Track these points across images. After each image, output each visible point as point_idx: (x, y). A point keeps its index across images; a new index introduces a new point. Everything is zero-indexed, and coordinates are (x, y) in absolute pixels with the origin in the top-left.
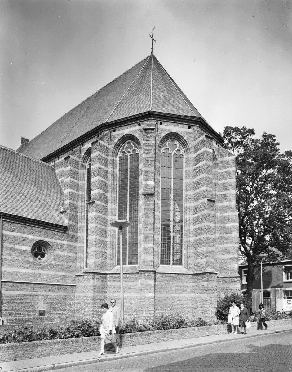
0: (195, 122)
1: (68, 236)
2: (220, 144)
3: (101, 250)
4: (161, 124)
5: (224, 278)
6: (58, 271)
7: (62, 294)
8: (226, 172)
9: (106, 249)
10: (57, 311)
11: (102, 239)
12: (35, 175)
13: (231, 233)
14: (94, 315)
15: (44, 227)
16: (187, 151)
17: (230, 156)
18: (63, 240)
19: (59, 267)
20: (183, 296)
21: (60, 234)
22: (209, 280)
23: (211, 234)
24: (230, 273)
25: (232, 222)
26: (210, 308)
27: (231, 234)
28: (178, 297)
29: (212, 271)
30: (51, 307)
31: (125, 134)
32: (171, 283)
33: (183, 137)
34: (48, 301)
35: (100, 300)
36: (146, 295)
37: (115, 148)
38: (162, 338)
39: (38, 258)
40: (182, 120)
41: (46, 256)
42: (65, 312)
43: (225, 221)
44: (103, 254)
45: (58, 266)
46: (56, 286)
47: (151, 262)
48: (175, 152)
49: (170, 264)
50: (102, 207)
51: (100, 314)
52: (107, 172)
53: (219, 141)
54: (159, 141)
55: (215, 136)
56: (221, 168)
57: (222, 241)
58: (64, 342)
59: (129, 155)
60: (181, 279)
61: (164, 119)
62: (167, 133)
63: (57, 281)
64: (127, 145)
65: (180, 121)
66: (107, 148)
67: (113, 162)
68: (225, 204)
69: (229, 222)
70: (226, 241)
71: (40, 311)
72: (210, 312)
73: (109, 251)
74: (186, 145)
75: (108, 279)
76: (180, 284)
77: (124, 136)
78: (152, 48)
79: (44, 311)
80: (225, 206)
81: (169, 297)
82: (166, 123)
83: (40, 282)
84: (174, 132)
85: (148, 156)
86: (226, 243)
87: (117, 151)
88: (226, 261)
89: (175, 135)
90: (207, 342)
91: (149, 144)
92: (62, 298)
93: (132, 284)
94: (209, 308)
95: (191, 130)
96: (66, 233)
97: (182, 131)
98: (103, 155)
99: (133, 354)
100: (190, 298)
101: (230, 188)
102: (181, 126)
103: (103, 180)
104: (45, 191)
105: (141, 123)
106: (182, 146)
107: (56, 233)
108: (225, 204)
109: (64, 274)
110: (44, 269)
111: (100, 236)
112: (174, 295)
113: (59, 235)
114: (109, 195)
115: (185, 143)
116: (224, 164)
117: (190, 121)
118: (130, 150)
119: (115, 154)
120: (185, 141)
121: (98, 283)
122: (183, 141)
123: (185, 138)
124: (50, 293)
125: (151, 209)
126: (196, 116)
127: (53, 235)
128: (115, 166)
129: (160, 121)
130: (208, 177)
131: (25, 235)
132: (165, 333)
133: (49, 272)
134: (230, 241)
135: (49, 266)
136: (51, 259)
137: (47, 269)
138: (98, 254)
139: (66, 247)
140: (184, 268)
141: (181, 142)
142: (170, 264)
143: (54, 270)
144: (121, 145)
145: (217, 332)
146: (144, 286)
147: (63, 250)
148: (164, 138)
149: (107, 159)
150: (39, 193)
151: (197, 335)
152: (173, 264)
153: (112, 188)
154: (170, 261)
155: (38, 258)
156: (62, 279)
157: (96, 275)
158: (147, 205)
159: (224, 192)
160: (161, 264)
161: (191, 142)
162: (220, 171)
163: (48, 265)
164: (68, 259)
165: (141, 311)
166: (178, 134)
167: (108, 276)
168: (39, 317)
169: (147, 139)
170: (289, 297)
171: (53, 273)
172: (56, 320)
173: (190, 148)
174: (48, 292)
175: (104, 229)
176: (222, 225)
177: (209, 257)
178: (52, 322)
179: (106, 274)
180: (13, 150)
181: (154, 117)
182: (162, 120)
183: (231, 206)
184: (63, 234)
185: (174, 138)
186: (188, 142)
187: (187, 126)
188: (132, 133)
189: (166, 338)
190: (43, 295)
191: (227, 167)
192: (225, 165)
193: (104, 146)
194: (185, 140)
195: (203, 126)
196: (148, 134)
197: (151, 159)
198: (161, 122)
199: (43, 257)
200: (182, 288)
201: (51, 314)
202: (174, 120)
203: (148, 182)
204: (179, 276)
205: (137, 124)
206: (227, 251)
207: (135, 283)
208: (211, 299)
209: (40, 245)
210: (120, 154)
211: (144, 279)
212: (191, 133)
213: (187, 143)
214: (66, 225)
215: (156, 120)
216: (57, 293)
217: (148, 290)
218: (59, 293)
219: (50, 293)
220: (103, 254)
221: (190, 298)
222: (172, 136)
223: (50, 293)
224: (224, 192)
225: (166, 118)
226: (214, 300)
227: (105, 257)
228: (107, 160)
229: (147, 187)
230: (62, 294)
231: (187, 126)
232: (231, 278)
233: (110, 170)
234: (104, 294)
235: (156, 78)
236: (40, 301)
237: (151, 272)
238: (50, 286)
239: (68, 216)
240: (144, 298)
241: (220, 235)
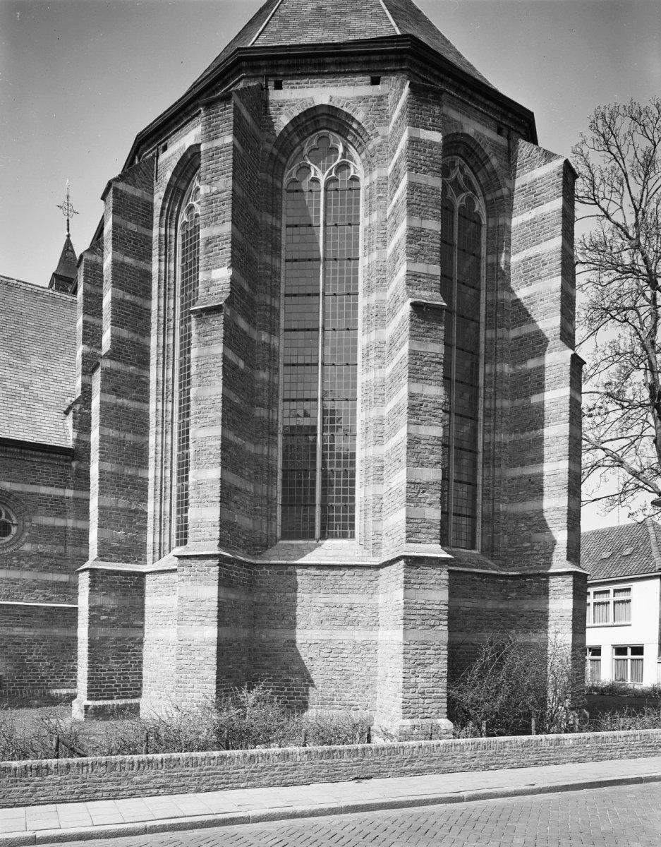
0: (392, 57)
6: (45, 570)
9: (143, 501)
12: (17, 323)
22: (412, 581)
29: (425, 552)
31: (187, 147)
33: (354, 115)
42: (67, 681)
43: (526, 387)
45: (45, 557)
48: (330, 173)
51: (116, 690)
54: (270, 142)
55: (488, 103)
61: (289, 66)
62: (296, 113)
65: (339, 64)
72: (416, 695)
76: (337, 599)
77: (185, 154)
84: (322, 106)
85: (214, 189)
89: (328, 115)
90: (549, 785)
91: (217, 148)
95: (379, 87)
97: (350, 97)
98: (132, 226)
100: (370, 646)
101: (545, 271)
102: (345, 81)
111: (120, 463)
117: (377, 58)
124: (16, 629)
129: (275, 79)
136: (23, 540)
137: (10, 565)
139: (71, 506)
143: (32, 566)
144: (183, 186)
147: (61, 514)
148: (291, 129)
161: (378, 129)
163: (12, 555)
166: (337, 109)
174: (12, 626)
184: (59, 470)
187: (367, 78)
194: (359, 124)
196: (214, 117)
197: (224, 195)
203: (213, 271)
211: (189, 583)
216: (42, 630)
217: (201, 619)
218: (47, 630)
219: (17, 631)
221: (370, 646)
229: (211, 289)
231: (367, 78)
237: (210, 562)
240: (188, 643)
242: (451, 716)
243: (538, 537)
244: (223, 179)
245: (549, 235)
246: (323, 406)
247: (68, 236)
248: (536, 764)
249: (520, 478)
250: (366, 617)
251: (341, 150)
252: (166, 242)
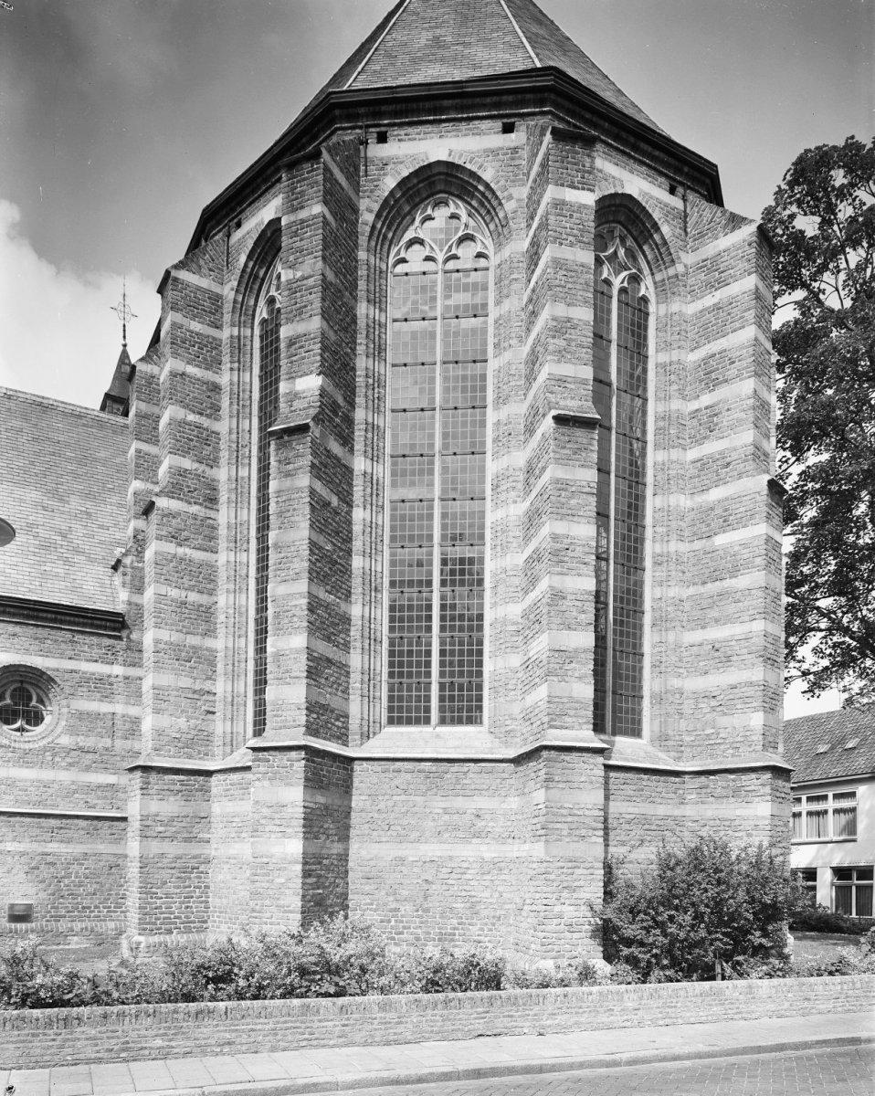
0: (528, 96)
1: (129, 648)
2: (689, 188)
3: (185, 682)
5: (703, 779)
6: (88, 769)
7: (101, 847)
8: (717, 307)
10: (83, 908)
11: (193, 640)
13: (734, 572)
14: (149, 923)
15: (28, 617)
16: (501, 233)
17: (733, 230)
18: (108, 663)
19: (90, 756)
20: (472, 854)
21: (95, 640)
22: (556, 778)
23: (574, 572)
24: (731, 751)
25: (743, 522)
26: (566, 908)
27: (734, 580)
28: (451, 858)
30: (59, 895)
32: (418, 799)
34: (45, 872)
35: (173, 871)
36: (29, 845)
37: (242, 290)
38: (159, 1042)
39: (18, 725)
40: (470, 101)
41: (48, 719)
43: (708, 525)
44: (196, 696)
46: (76, 821)
47: (298, 712)
49: (427, 721)
50: (190, 521)
52: (216, 388)
53: (687, 175)
54: (371, 211)
55: (657, 153)
56: (694, 295)
57: (698, 614)
58: (446, 1002)
60: (465, 781)
61: (396, 114)
62: (405, 173)
63: (81, 804)
65: (462, 109)
66: (217, 299)
67: (238, 346)
68: (711, 447)
69: (726, 525)
70: (714, 613)
71: (12, 906)
73: (221, 687)
74: (494, 209)
75: (214, 791)
76: (459, 803)
77: (264, 232)
79: (30, 907)
80: (711, 456)
81: (411, 859)
82: (402, 132)
83: (13, 806)
84: (439, 162)
85: (299, 274)
86: (717, 621)
87: (252, 302)
88: (714, 703)
91: (303, 221)
92: (102, 864)
94: (557, 909)
95: (513, 136)
96: (120, 638)
99: (625, 1057)
101: (733, 372)
103: (191, 417)
104: (75, 503)
106: (481, 215)
107: (78, 637)
108: (711, 447)
109: (112, 779)
110: (28, 765)
111: (181, 631)
112: (432, 850)
113: (91, 643)
114: (222, 474)
115: (489, 202)
116: (710, 271)
117: (510, 98)
119: (243, 312)
120: (487, 193)
121: (169, 807)
122: (483, 194)
123: (487, 176)
124: (50, 845)
125: (299, 490)
127: (63, 646)
128: (245, 362)
129: (378, 130)
130: (569, 320)
132: (181, 1016)
133: (47, 775)
134: (732, 608)
135: (48, 754)
138: (172, 699)
139: (119, 687)
140: (488, 735)
141: (474, 203)
142: (427, 721)
143: (71, 765)
144: (262, 273)
145: (549, 1022)
146: (265, 811)
147: (108, 697)
149: (214, 339)
150: (44, 508)
151: (406, 1031)
152: (443, 721)
153: (234, 446)
154: (428, 710)
155: (18, 725)
156: (105, 798)
157: (153, 777)
159: (706, 399)
160: (391, 721)
161: (512, 190)
162: (691, 309)
163: (45, 749)
164: (128, 726)
165: (255, 914)
166: (459, 166)
167: (214, 779)
168: (6, 928)
169: (295, 203)
171: (65, 776)
172: (76, 938)
173: (510, 216)
175: (201, 605)
176: (698, 545)
177: (563, 677)
178: (61, 947)
179: (209, 773)
180: (43, 398)
181: (349, 118)
182: (386, 122)
183: (734, 456)
185: (446, 193)
186: (498, 193)
187: (498, 124)
189: (180, 1044)
190: (23, 854)
192: (715, 273)
193: (199, 288)
194: (487, 186)
195: (578, 109)
196: (298, 182)
197: (311, 282)
198: (383, 129)
199: (36, 724)
201: (57, 918)
202: (435, 111)
204: (456, 767)
206: (721, 655)
208: (570, 864)
209: (22, 682)
211: (266, 783)
212: (515, 150)
213: (497, 198)
214: (120, 608)
215: (361, 128)
217: (282, 829)
218: (89, 846)
219: (53, 847)
220: (196, 696)
221: (502, 864)
222: (434, 182)
223: (53, 847)
224: (706, 399)
225: (399, 107)
226: (585, 872)
227: (203, 708)
228: (216, 345)
229: (295, 403)
230: (101, 847)
231: (498, 124)
232: (732, 777)
233: (225, 378)
234: (194, 849)
236: (14, 871)
237: (293, 754)
238: (53, 822)
239: (128, 578)
240: (265, 860)
241: (692, 590)
244: (309, 261)
245: (737, 325)
247: (125, 346)
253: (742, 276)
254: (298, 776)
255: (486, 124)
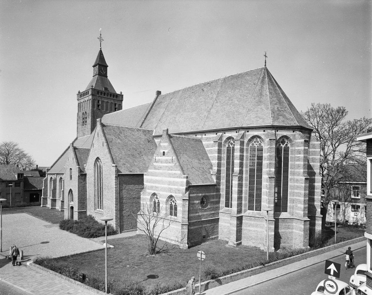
4: (277, 131)
49: (253, 210)
59: (256, 146)
62: (280, 136)
64: (255, 140)
76: (286, 224)
78: (265, 63)
85: (271, 154)
93: (258, 223)
101: (316, 161)
105: (265, 130)
118: (257, 143)
123: (291, 138)
126: (299, 125)
131: (198, 195)
133: (207, 213)
158: (271, 183)
160: (248, 210)
170: (356, 210)
187: (292, 131)
188: (259, 135)
191: (315, 148)
200: (288, 226)
205: (263, 130)
207: (260, 223)
210: (251, 145)
231: (292, 131)
235: (271, 91)
242: (309, 246)
243: (314, 209)
244: (273, 153)
245: (317, 155)
246: (250, 164)
247: (101, 48)
248: (323, 253)
249: (311, 198)
250: (291, 227)
251: (286, 142)
252: (247, 150)
253: (318, 148)
254: (235, 225)
255: (291, 131)
